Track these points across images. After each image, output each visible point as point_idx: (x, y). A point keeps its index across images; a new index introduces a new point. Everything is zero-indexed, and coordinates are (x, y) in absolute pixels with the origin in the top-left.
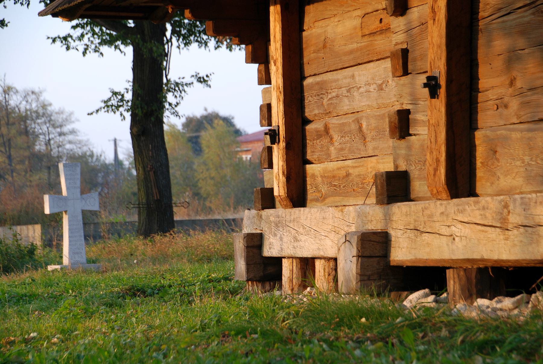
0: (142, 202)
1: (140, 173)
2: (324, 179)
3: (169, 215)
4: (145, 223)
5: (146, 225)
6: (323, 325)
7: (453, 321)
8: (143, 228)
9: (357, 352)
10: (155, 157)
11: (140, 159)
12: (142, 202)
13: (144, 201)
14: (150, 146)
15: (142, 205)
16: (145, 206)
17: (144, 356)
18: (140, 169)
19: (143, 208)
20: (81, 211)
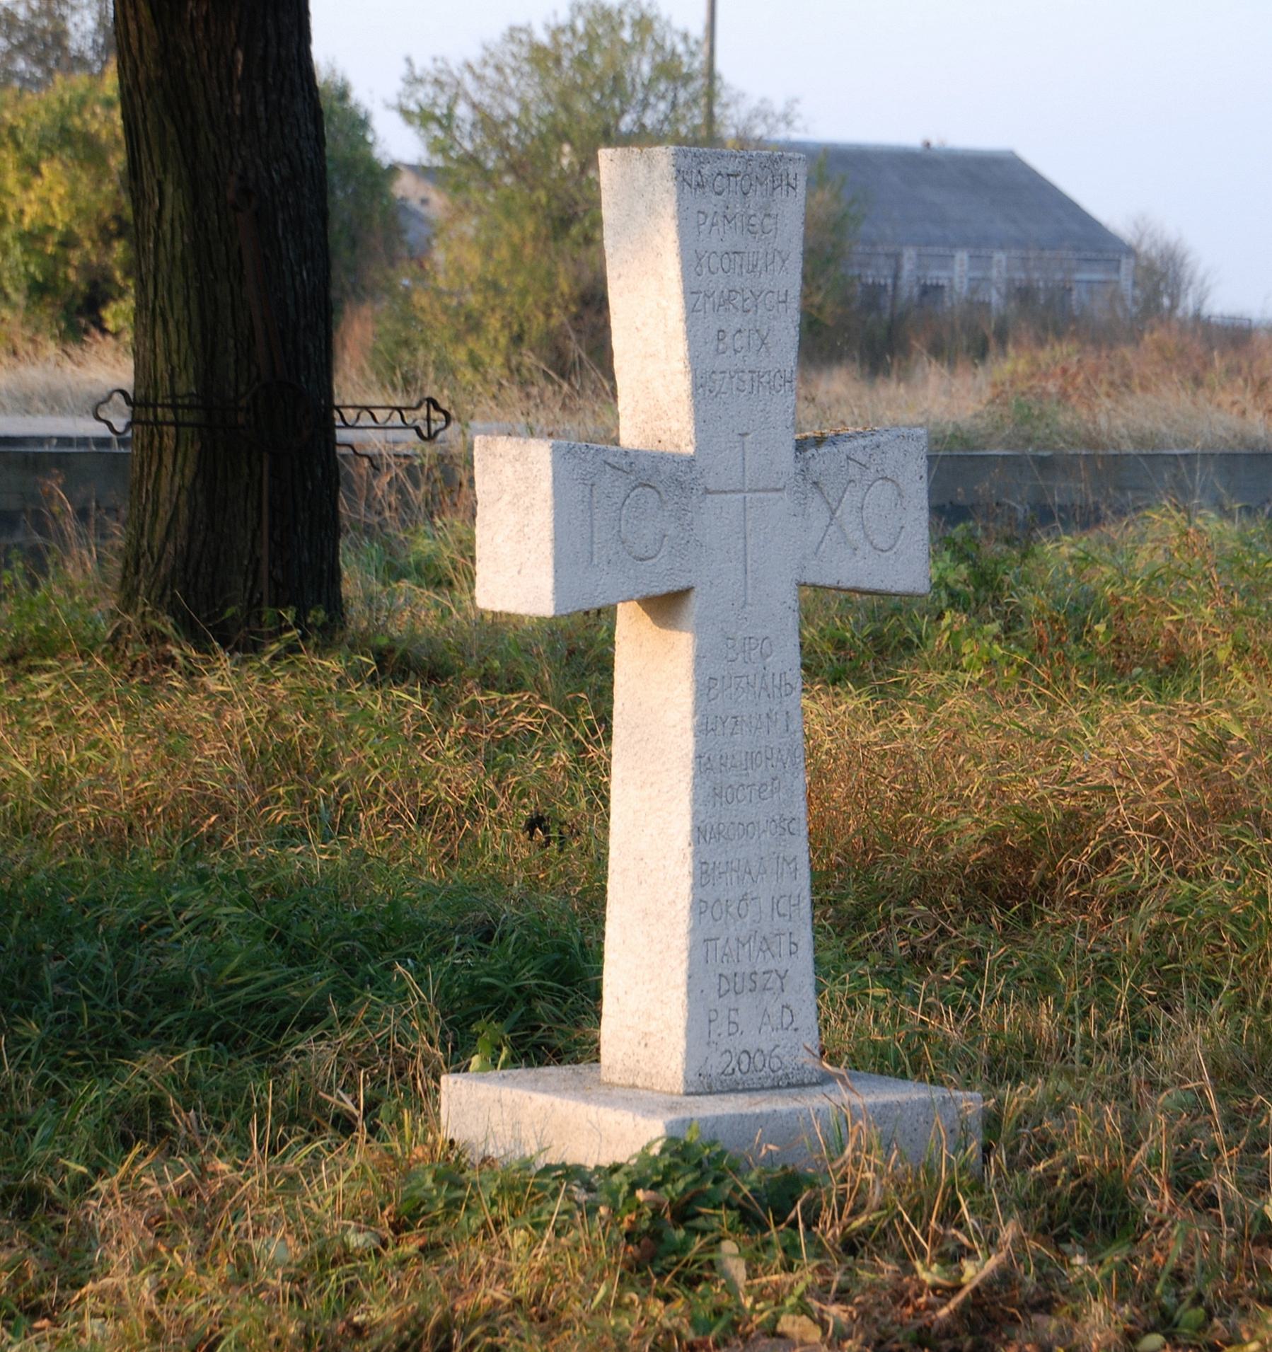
0: (173, 395)
1: (167, 214)
2: (627, 123)
3: (319, 472)
4: (184, 514)
5: (191, 529)
6: (159, 870)
7: (824, 196)
8: (170, 547)
9: (145, 858)
10: (263, 125)
11: (171, 130)
12: (173, 395)
13: (185, 385)
14: (240, 55)
15: (174, 407)
16: (190, 417)
17: (462, 355)
18: (169, 189)
19: (177, 424)
20: (789, 597)
